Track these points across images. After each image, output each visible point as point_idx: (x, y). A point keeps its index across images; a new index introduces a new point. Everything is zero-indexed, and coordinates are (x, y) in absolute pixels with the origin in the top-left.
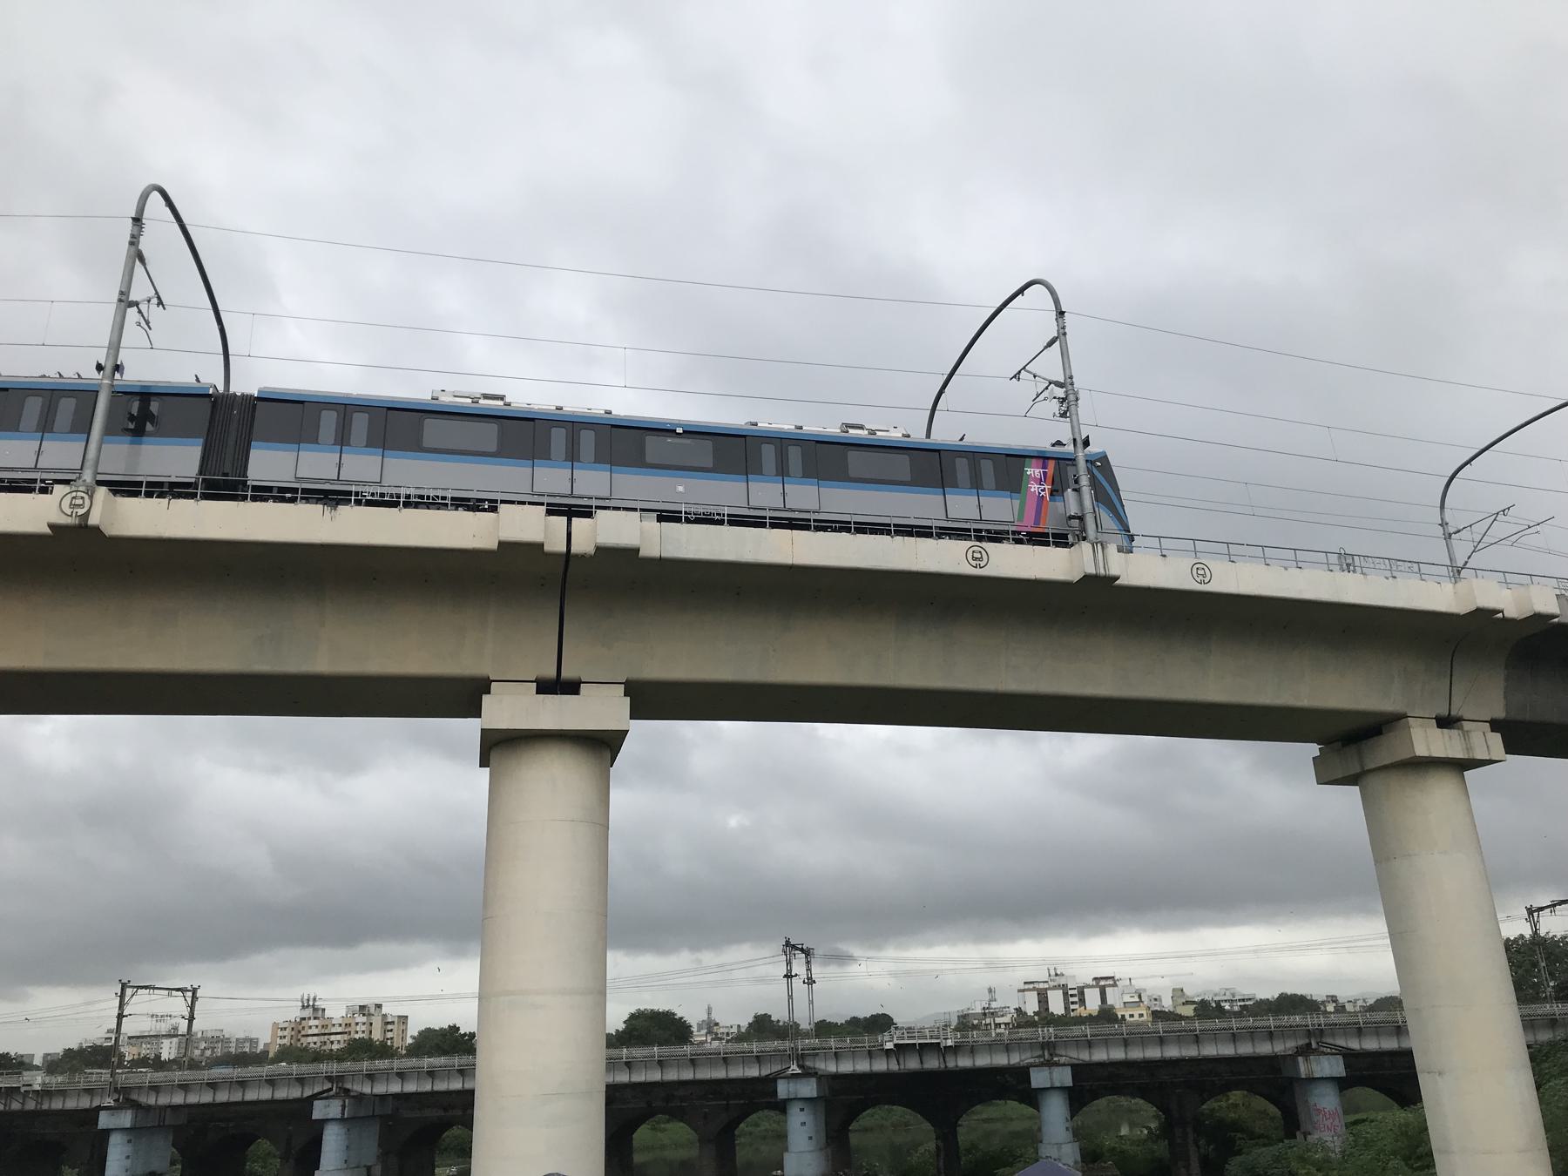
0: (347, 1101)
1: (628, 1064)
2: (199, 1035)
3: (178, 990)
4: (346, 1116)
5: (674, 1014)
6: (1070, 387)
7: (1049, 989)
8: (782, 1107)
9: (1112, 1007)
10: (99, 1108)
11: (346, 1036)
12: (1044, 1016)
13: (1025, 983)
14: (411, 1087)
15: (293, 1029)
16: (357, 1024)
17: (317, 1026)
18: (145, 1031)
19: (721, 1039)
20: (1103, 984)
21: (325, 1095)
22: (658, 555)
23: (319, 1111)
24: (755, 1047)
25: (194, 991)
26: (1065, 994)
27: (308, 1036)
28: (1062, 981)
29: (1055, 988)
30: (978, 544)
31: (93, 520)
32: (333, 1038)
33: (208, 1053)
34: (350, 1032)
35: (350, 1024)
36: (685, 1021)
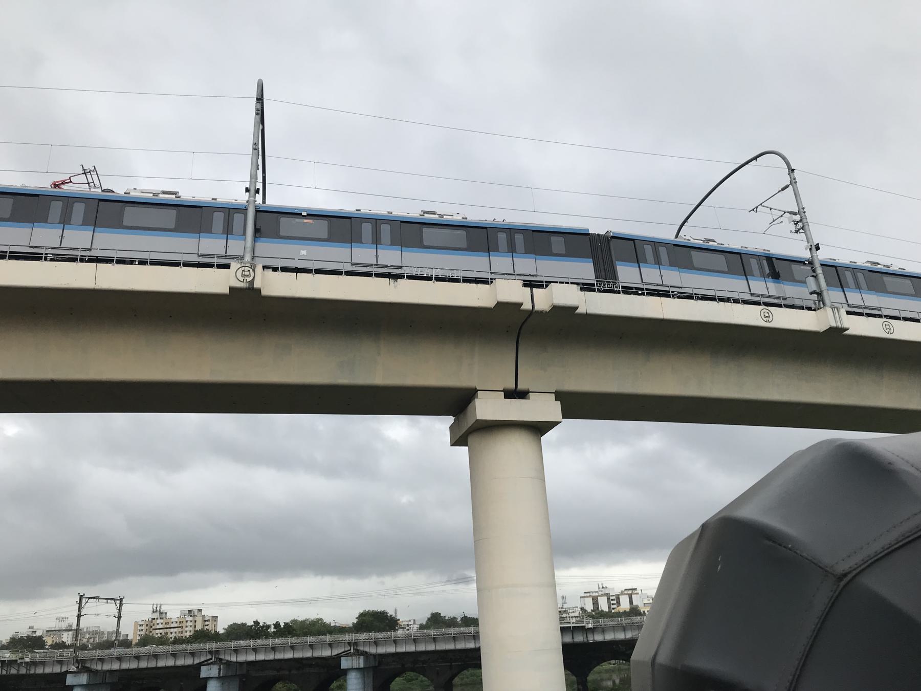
0: (222, 666)
1: (395, 641)
2: (85, 630)
3: (112, 599)
4: (221, 675)
5: (387, 613)
6: (803, 214)
7: (599, 596)
8: (345, 672)
9: (637, 606)
10: (67, 672)
11: (180, 629)
12: (597, 614)
13: (585, 593)
14: (261, 657)
15: (147, 625)
16: (187, 621)
17: (162, 624)
18: (52, 628)
19: (404, 628)
20: (631, 593)
21: (206, 663)
22: (585, 312)
23: (204, 672)
24: (432, 632)
25: (121, 600)
26: (608, 599)
27: (156, 629)
28: (607, 592)
29: (602, 595)
30: (766, 307)
31: (257, 285)
32: (172, 630)
33: (92, 640)
34: (182, 627)
35: (182, 622)
36: (325, 623)
